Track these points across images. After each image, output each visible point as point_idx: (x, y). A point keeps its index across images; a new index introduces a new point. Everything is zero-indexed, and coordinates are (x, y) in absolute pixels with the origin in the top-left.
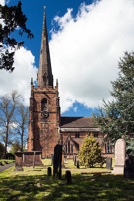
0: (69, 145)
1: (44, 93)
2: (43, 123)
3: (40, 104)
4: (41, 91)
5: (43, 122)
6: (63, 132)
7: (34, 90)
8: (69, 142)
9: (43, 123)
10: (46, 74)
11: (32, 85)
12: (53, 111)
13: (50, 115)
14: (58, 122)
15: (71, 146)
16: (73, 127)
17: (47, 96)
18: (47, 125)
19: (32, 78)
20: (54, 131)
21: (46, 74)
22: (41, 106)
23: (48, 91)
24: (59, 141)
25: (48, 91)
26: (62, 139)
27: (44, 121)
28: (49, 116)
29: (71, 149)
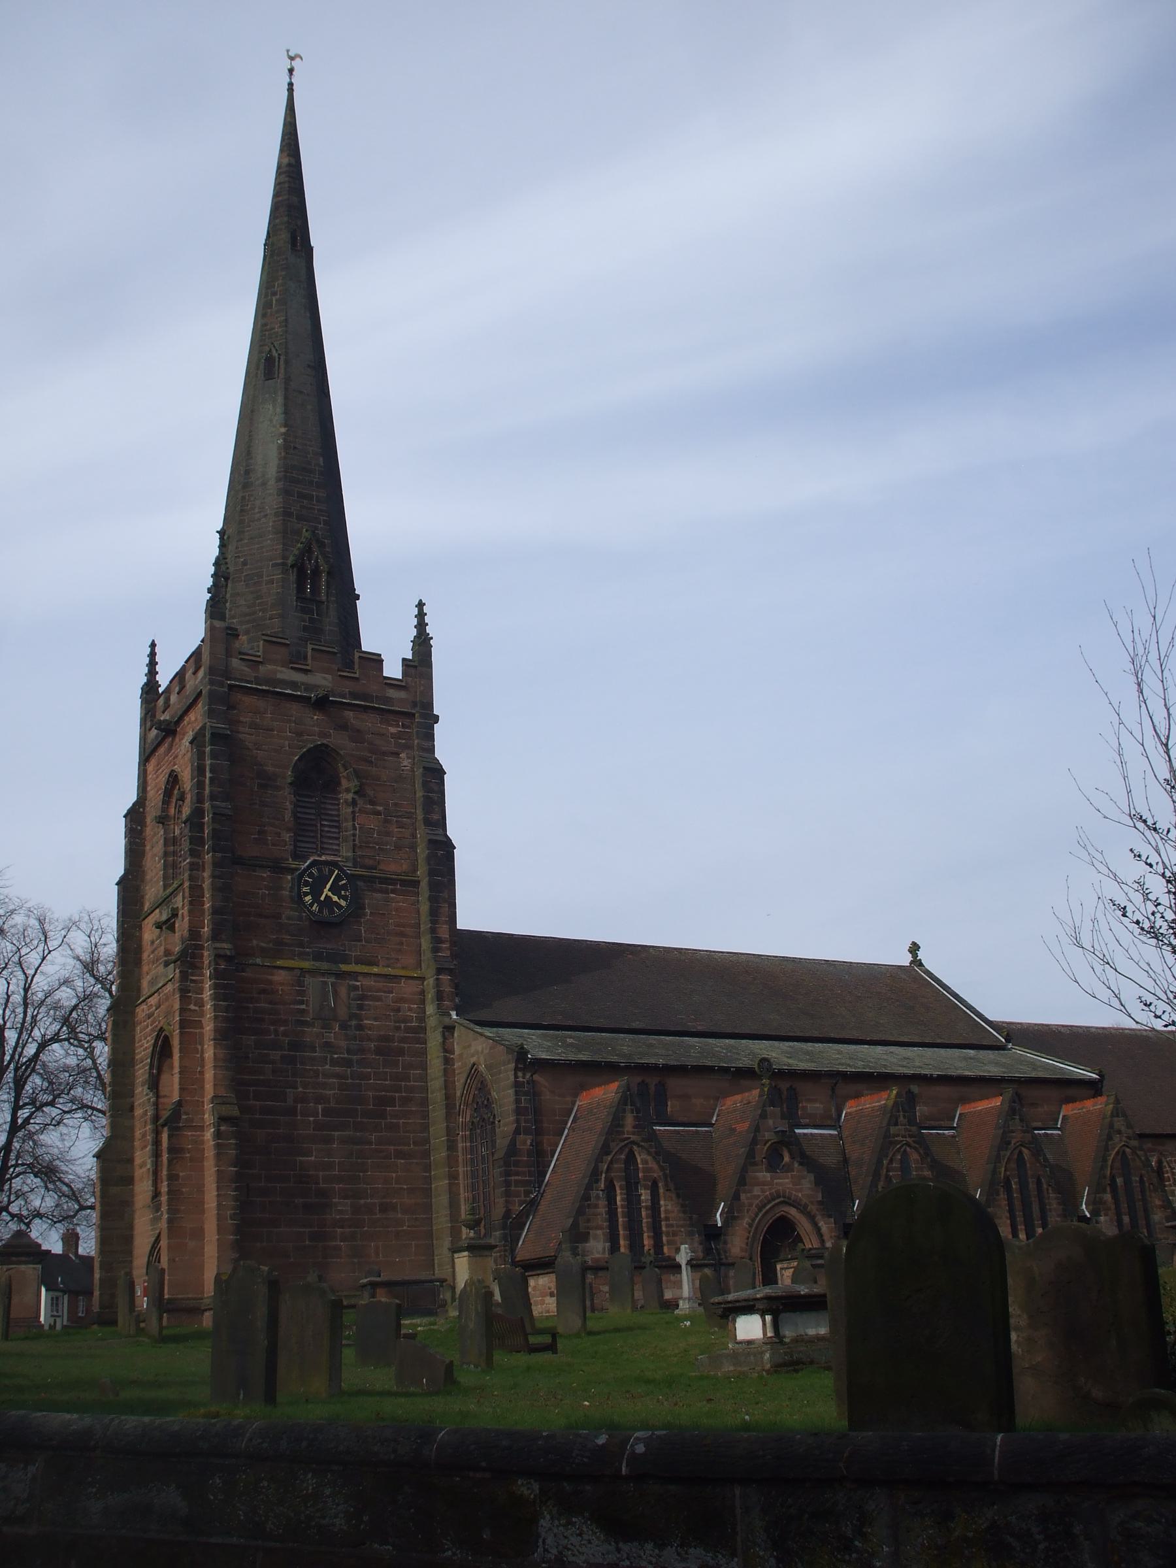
0: (631, 1188)
1: (322, 704)
2: (312, 972)
3: (286, 799)
4: (294, 685)
5: (306, 965)
6: (540, 1065)
7: (235, 662)
8: (631, 1158)
9: (312, 972)
10: (321, 545)
11: (218, 624)
12: (393, 868)
13: (372, 899)
14: (450, 971)
15: (645, 1195)
16: (917, 1039)
17: (344, 727)
18: (343, 991)
19: (420, 605)
20: (401, 1052)
21: (321, 545)
22: (288, 816)
23: (354, 695)
24: (513, 1143)
25: (354, 695)
26: (539, 1132)
27: (318, 957)
28: (357, 908)
29: (645, 1220)
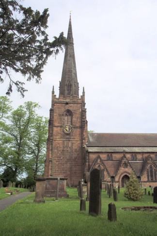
27: (67, 138)
